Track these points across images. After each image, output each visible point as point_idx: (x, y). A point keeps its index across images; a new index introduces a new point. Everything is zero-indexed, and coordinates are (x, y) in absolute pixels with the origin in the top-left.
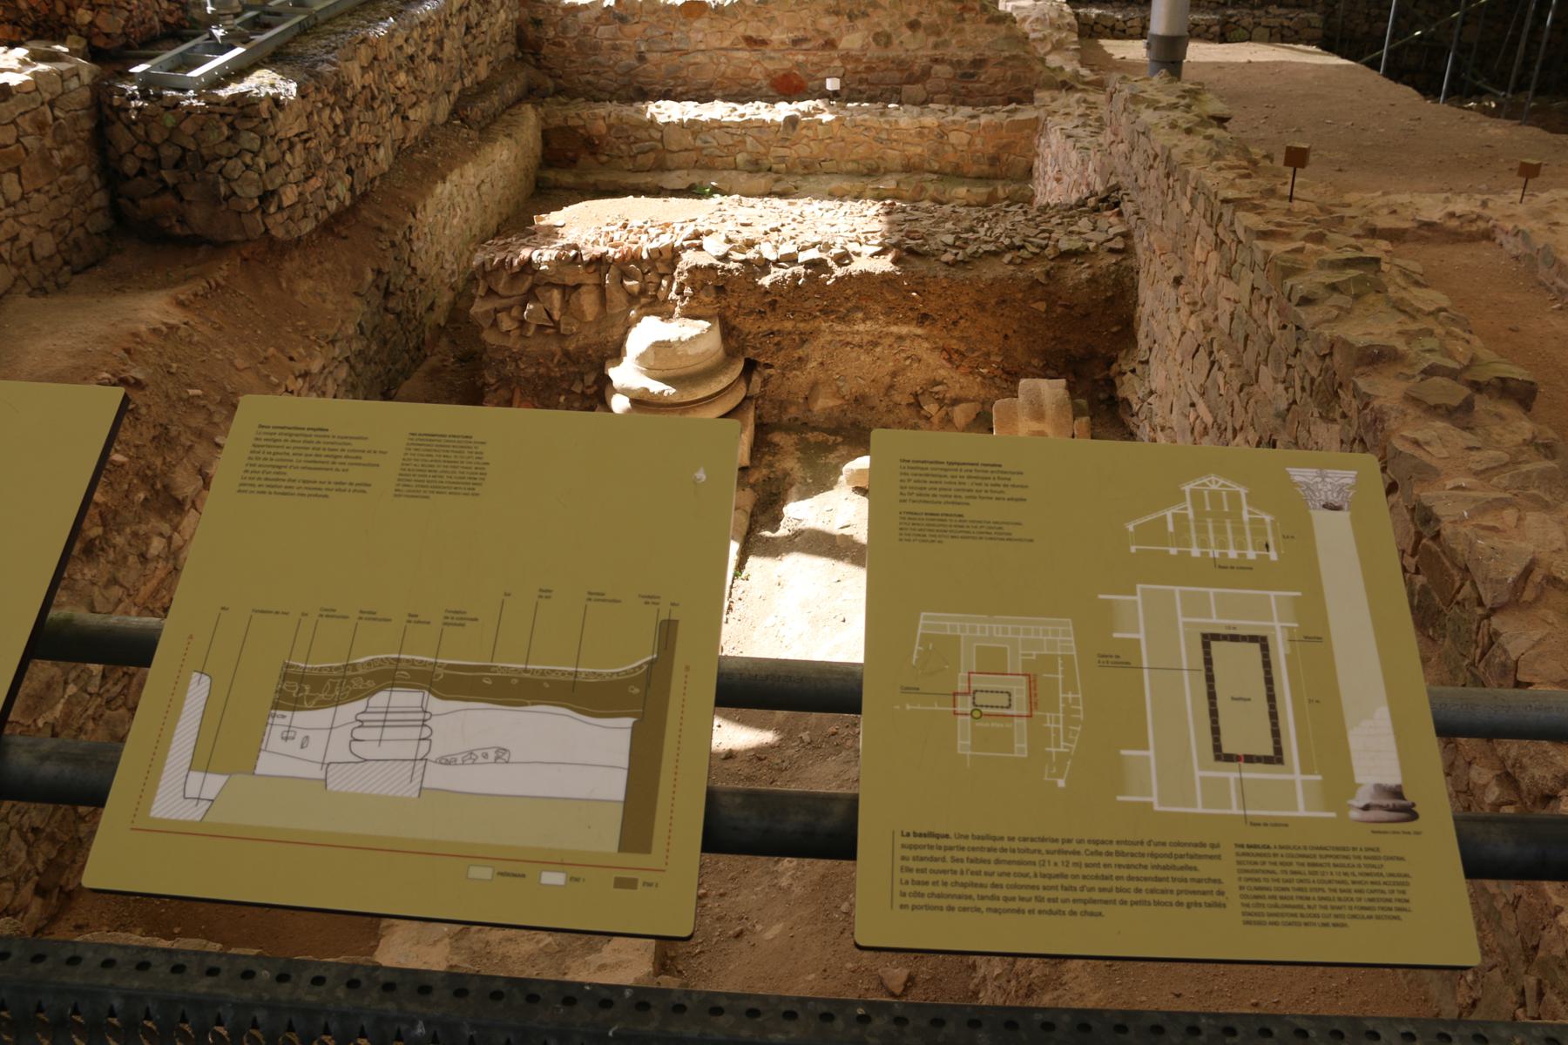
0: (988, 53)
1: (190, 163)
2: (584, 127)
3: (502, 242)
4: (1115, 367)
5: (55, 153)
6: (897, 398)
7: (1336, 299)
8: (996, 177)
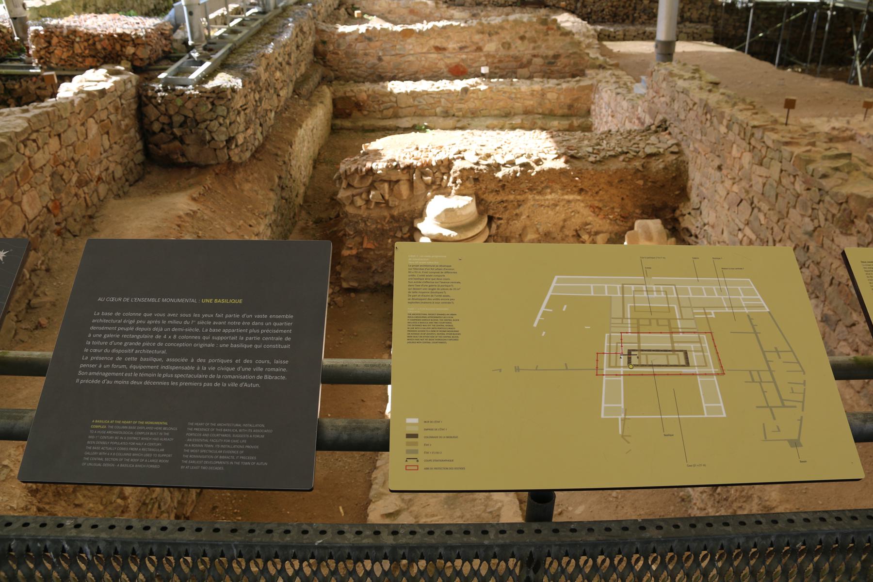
0: (561, 51)
1: (189, 124)
2: (355, 96)
3: (352, 159)
4: (678, 213)
5: (122, 122)
6: (567, 232)
7: (838, 174)
8: (571, 116)
